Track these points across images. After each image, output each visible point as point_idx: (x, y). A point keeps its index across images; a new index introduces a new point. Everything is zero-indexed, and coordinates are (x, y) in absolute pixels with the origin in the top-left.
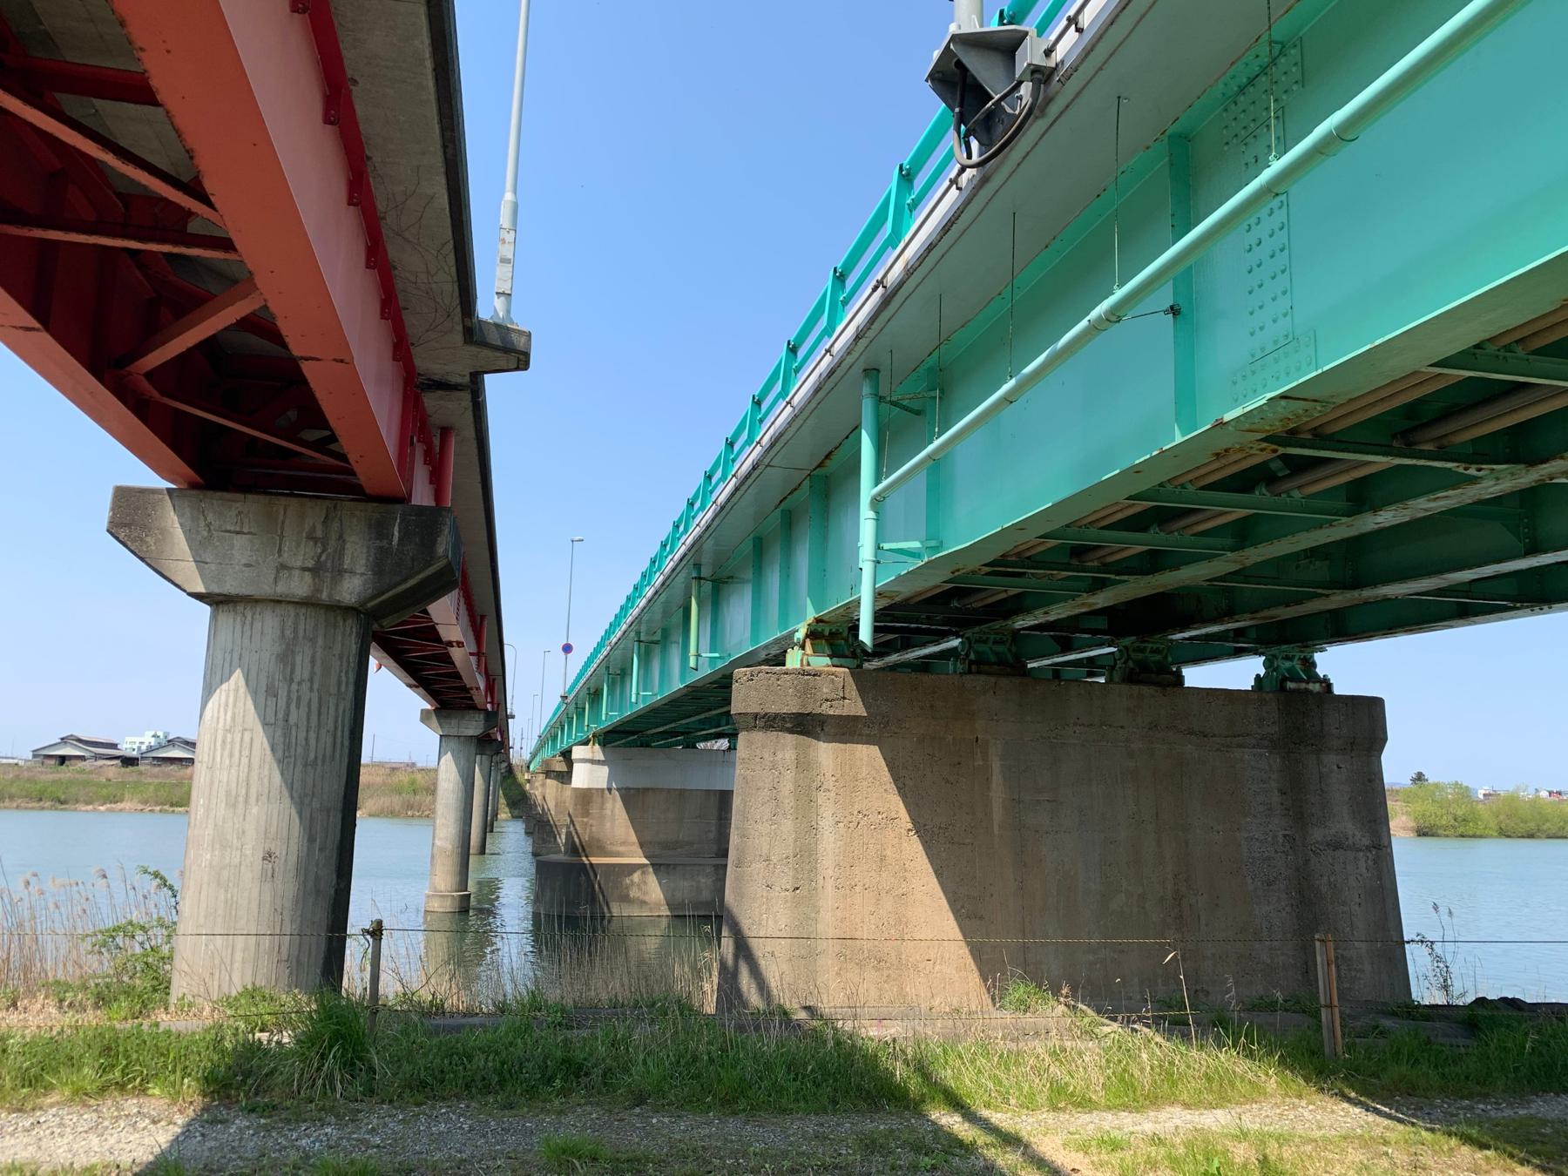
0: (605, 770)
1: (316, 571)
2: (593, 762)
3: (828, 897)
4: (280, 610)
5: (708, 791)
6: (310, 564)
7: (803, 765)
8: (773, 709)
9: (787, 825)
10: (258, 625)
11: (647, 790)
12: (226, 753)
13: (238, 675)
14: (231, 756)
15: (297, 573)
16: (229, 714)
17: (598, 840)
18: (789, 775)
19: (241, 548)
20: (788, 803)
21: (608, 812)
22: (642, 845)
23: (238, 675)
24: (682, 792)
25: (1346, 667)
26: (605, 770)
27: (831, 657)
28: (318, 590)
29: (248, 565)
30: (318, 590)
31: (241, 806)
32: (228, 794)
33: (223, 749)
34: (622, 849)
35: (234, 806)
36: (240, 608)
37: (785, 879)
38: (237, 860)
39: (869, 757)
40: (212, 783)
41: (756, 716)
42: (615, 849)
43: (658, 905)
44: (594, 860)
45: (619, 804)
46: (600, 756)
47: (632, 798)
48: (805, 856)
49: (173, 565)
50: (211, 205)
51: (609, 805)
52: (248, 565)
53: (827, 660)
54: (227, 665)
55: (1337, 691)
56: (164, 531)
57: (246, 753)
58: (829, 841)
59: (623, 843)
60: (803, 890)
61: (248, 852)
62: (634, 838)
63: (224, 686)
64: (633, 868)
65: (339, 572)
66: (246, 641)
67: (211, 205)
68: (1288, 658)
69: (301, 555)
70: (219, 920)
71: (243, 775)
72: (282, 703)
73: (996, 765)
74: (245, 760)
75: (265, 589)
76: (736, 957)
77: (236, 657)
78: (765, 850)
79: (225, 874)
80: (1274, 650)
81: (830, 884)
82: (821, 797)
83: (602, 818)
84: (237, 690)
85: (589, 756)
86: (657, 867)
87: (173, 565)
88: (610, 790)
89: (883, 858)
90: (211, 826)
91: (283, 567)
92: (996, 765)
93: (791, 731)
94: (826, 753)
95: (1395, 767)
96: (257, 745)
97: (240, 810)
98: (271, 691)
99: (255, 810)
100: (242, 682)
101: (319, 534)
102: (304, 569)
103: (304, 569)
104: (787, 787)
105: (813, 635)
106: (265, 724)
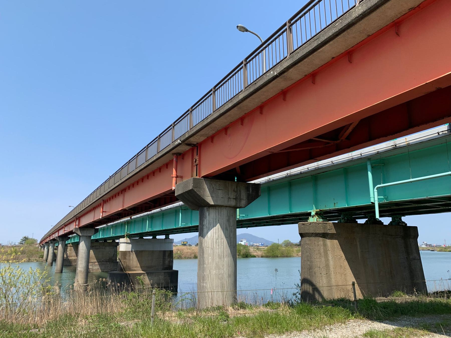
0: (130, 246)
1: (236, 199)
2: (127, 243)
3: (333, 276)
4: (227, 208)
5: (160, 251)
6: (235, 197)
7: (325, 245)
8: (318, 232)
9: (323, 259)
10: (222, 212)
11: (142, 251)
12: (217, 245)
13: (218, 225)
14: (219, 246)
15: (232, 199)
16: (217, 235)
17: (128, 266)
18: (322, 247)
19: (220, 193)
20: (323, 254)
21: (131, 258)
22: (141, 267)
23: (218, 225)
24: (153, 252)
25: (409, 220)
26: (130, 246)
27: (323, 219)
28: (237, 204)
29: (222, 198)
30: (237, 204)
31: (222, 258)
32: (219, 255)
33: (216, 244)
34: (135, 269)
35: (221, 258)
36: (217, 208)
37: (324, 272)
38: (223, 272)
39: (336, 242)
40: (214, 253)
41: (312, 233)
42: (133, 269)
43: (148, 285)
44: (130, 272)
45: (135, 255)
46: (129, 241)
47: (139, 254)
48: (327, 266)
49: (207, 197)
50: (351, 124)
51: (132, 256)
52: (222, 198)
53: (322, 220)
54: (215, 222)
55: (408, 225)
56: (204, 189)
57: (222, 245)
58: (331, 263)
59: (136, 267)
60: (328, 275)
61: (225, 270)
62: (139, 265)
63: (215, 228)
64: (140, 274)
65: (241, 199)
66: (220, 216)
67: (351, 124)
68: (397, 218)
69: (232, 195)
70: (220, 288)
71: (222, 250)
72: (229, 232)
73: (358, 243)
74: (222, 247)
75: (226, 203)
76: (313, 291)
77: (217, 220)
78: (319, 265)
79: (220, 276)
80: (395, 216)
81: (333, 272)
82: (329, 252)
83: (130, 260)
84: (218, 229)
85: (126, 241)
86: (148, 274)
87: (207, 197)
88: (132, 251)
89: (341, 266)
90: (214, 264)
91: (229, 198)
92: (358, 243)
93: (321, 237)
94: (328, 242)
95: (421, 241)
96: (225, 243)
97: (222, 260)
98: (226, 229)
99: (226, 259)
100: (220, 227)
101: (236, 190)
102: (234, 199)
103: (234, 199)
104: (322, 251)
105: (317, 214)
106: (226, 237)
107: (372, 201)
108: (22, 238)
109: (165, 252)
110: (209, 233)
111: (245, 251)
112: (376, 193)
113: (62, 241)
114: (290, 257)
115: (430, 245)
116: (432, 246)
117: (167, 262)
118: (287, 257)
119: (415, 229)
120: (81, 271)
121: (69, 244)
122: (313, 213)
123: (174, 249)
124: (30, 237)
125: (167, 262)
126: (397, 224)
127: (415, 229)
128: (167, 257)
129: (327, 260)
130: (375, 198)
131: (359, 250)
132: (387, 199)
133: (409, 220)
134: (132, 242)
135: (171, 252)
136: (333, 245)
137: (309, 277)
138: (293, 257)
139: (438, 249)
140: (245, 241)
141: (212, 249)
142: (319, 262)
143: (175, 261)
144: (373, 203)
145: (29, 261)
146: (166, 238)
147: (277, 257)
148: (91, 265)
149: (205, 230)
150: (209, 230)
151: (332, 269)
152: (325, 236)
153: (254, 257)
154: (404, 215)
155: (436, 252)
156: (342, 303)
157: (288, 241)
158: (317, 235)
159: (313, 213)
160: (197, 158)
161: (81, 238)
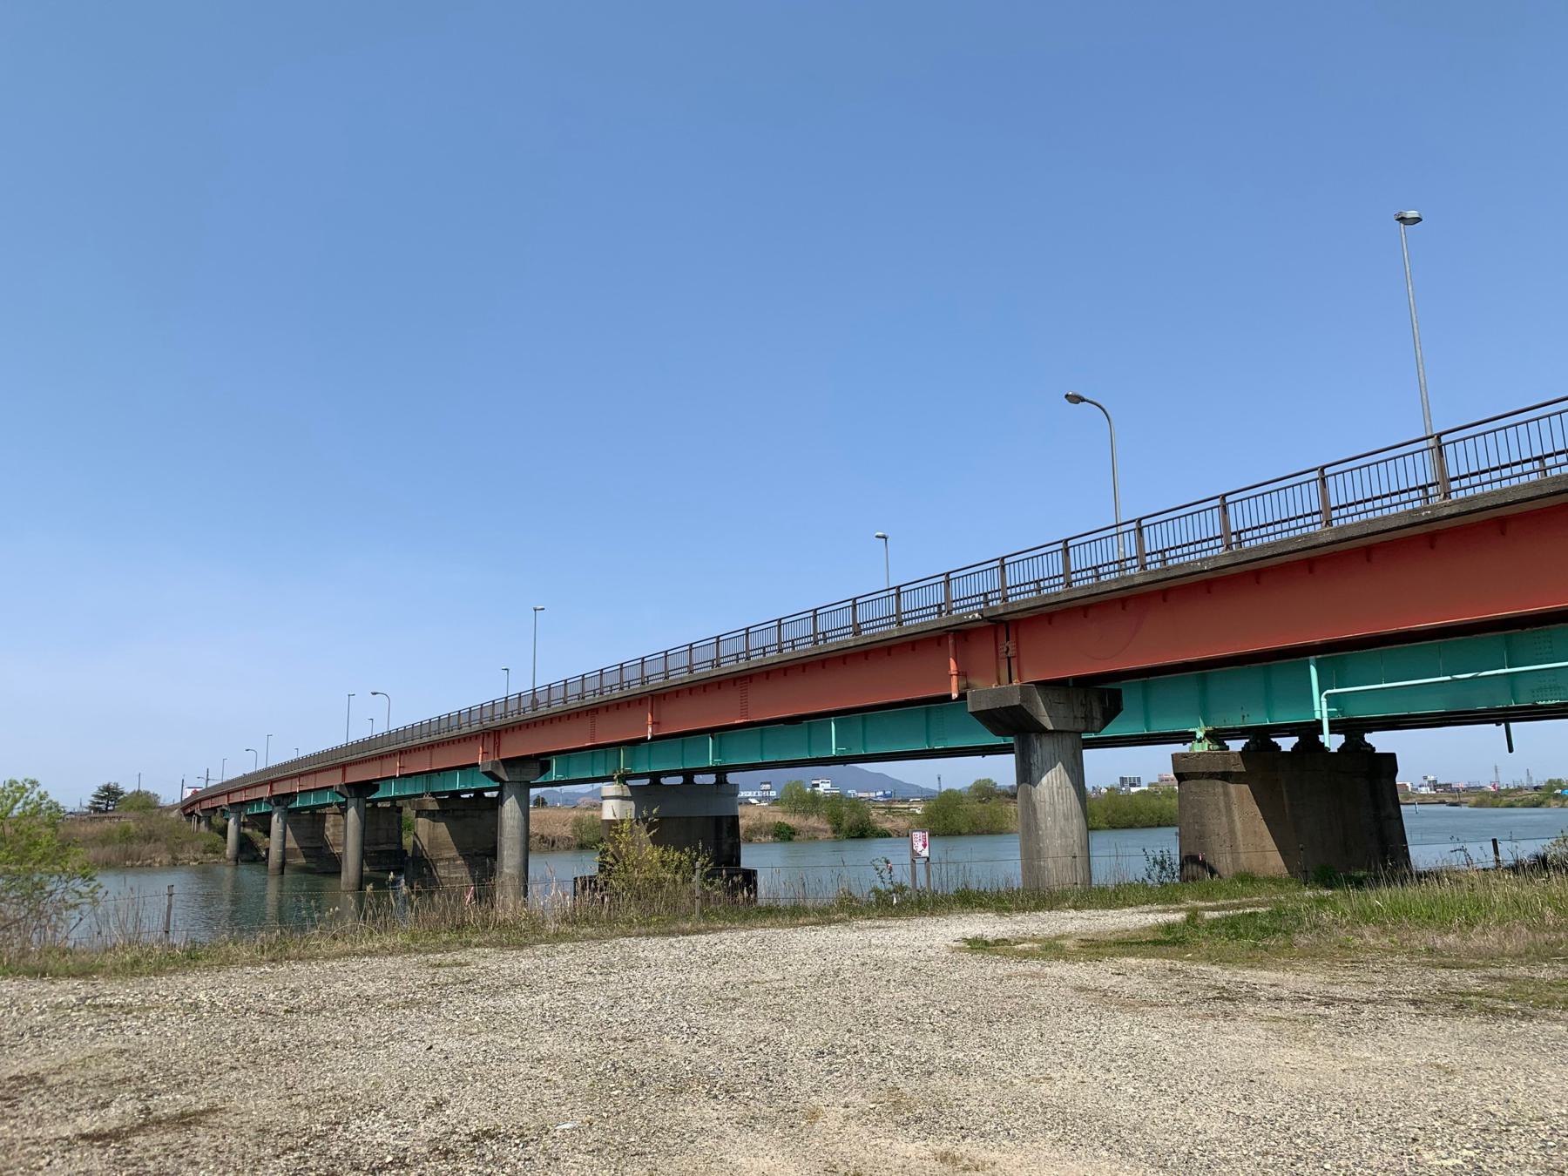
0: (632, 805)
1: (1085, 718)
7: (1226, 794)
9: (1224, 819)
25: (1380, 741)
26: (632, 805)
39: (1246, 787)
48: (1232, 832)
58: (1238, 825)
85: (619, 793)
94: (1232, 788)
95: (1405, 777)
104: (1222, 804)
105: (1207, 735)
107: (1318, 716)
108: (95, 790)
109: (718, 820)
110: (1044, 780)
111: (855, 816)
112: (1324, 705)
113: (358, 797)
114: (1000, 832)
115: (1447, 787)
116: (1452, 790)
117: (725, 847)
118: (990, 833)
119: (1390, 759)
120: (512, 877)
121: (330, 805)
122: (1200, 734)
123: (741, 810)
124: (128, 788)
125: (725, 847)
126: (1356, 748)
127: (1390, 759)
128: (725, 835)
129: (1231, 821)
130: (1321, 710)
131: (1286, 802)
132: (1342, 713)
133: (1380, 741)
134: (637, 795)
135: (735, 819)
136: (1240, 793)
137: (1193, 851)
138: (1010, 833)
139: (1473, 800)
140: (828, 786)
141: (1053, 804)
142: (1216, 825)
143: (743, 847)
144: (1320, 722)
145: (175, 863)
146: (718, 782)
147: (960, 834)
148: (444, 867)
149: (1035, 774)
150: (1043, 773)
151: (1239, 834)
152: (1226, 777)
153: (886, 834)
154: (1370, 731)
155: (1465, 808)
156: (1272, 880)
157: (990, 781)
158: (1212, 776)
159: (1200, 734)
160: (1011, 644)
161: (506, 788)
